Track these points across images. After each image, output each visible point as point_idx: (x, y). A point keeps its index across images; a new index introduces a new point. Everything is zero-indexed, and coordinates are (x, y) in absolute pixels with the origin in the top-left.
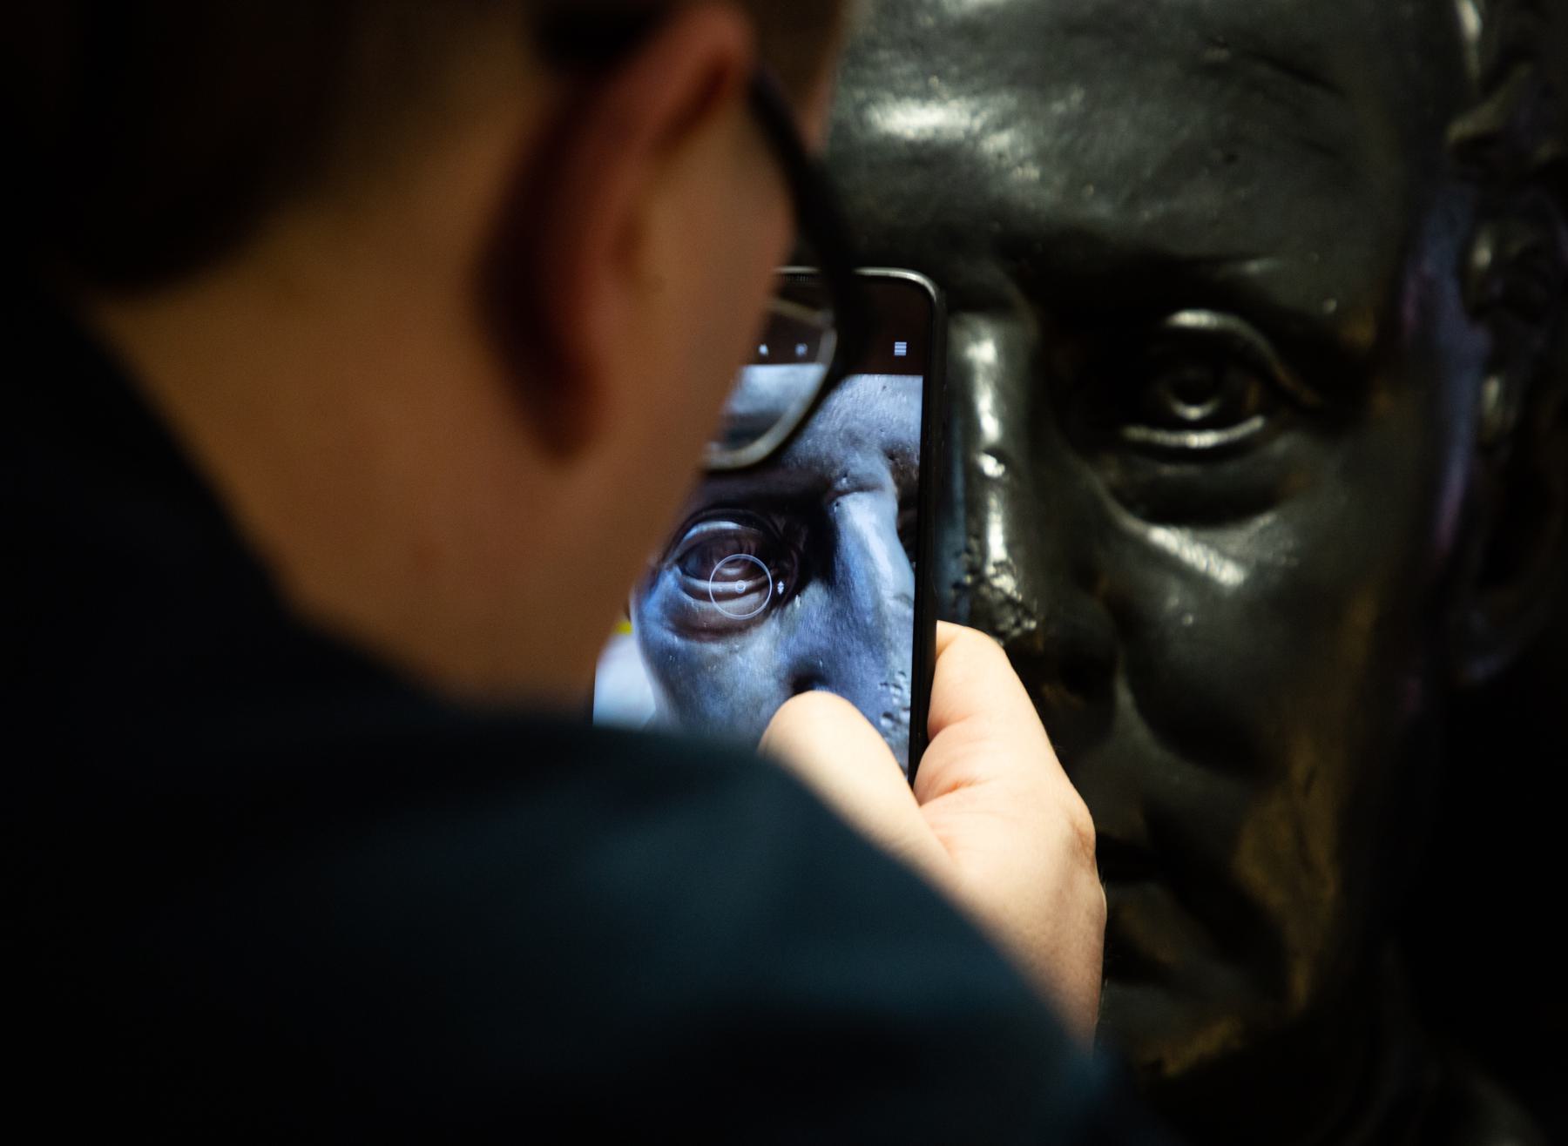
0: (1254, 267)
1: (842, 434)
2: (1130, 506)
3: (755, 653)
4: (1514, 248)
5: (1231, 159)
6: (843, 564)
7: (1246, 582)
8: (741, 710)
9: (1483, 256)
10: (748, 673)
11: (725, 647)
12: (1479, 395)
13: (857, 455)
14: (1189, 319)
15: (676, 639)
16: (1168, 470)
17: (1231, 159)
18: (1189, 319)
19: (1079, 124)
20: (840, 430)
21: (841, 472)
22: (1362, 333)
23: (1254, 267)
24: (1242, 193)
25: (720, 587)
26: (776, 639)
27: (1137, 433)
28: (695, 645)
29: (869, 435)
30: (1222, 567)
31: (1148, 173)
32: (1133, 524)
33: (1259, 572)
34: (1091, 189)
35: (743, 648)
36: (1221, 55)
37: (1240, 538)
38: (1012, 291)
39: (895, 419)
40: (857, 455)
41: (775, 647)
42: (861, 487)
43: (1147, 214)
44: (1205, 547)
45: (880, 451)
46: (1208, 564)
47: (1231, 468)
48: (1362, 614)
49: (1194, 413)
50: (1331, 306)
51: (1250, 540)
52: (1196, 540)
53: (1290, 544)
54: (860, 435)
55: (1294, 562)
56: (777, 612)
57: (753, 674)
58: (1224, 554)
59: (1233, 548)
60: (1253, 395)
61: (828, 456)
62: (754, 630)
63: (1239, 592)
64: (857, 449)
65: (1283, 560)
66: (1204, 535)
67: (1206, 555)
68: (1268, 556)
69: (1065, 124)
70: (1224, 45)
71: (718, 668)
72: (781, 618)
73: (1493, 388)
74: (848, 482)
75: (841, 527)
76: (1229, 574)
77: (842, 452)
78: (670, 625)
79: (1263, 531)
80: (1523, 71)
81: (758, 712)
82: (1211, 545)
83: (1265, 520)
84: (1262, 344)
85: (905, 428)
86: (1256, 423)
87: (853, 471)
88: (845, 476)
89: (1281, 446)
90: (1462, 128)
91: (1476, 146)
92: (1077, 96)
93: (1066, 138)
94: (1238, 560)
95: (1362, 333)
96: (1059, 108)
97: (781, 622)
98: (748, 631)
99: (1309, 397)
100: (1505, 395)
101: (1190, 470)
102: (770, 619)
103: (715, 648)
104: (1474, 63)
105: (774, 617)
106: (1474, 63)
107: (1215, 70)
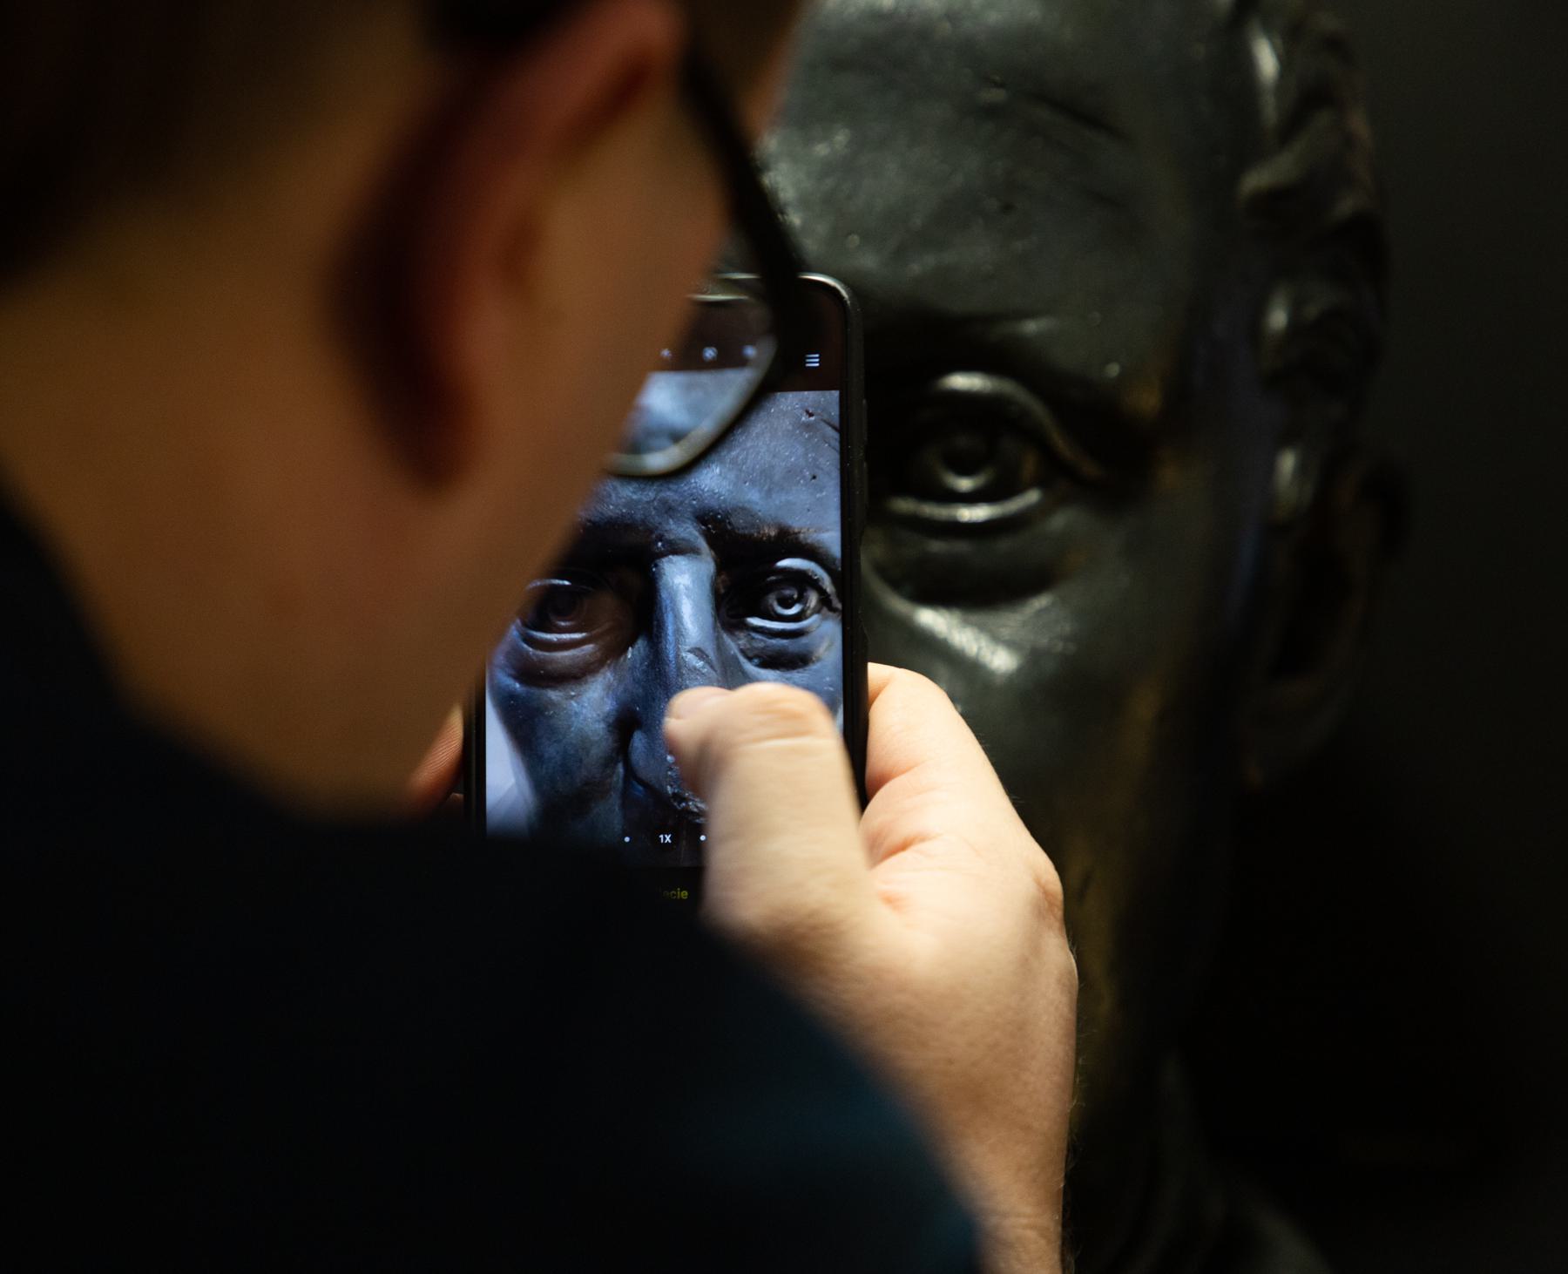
0: (1031, 327)
1: (656, 503)
2: (896, 585)
3: (589, 699)
4: (1312, 311)
5: (1007, 208)
6: (658, 621)
7: (1020, 670)
8: (572, 752)
9: (1278, 318)
10: (581, 718)
11: (561, 694)
12: (1270, 468)
13: (671, 521)
14: (961, 381)
15: (518, 685)
16: (937, 546)
17: (1007, 208)
18: (961, 381)
19: (845, 167)
20: (655, 499)
21: (657, 537)
22: (1147, 400)
23: (1031, 327)
24: (1019, 245)
25: (553, 637)
26: (609, 687)
27: (904, 505)
28: (535, 691)
29: (682, 502)
30: (993, 653)
31: (917, 221)
32: (898, 604)
33: (1033, 658)
34: (855, 239)
35: (578, 695)
36: (996, 95)
37: (1014, 620)
38: (702, 544)
39: (706, 489)
40: (671, 521)
41: (608, 694)
42: (677, 549)
43: (919, 266)
44: (976, 631)
45: (692, 518)
46: (980, 649)
47: (1004, 545)
48: (1144, 706)
49: (965, 484)
50: (1114, 370)
51: (1024, 624)
52: (966, 623)
53: (1067, 628)
54: (673, 504)
55: (1072, 648)
56: (611, 662)
57: (585, 720)
58: (996, 639)
59: (1005, 632)
60: (1030, 465)
61: (643, 522)
62: (590, 679)
63: (1011, 679)
64: (671, 516)
65: (1060, 646)
66: (975, 618)
67: (977, 640)
68: (1044, 641)
69: (828, 169)
70: (1001, 85)
71: (555, 712)
72: (615, 668)
73: (1287, 463)
74: (663, 545)
75: (661, 583)
76: (1001, 661)
77: (657, 519)
78: (513, 672)
79: (1040, 612)
80: (1323, 119)
81: (588, 755)
82: (982, 628)
83: (1041, 602)
84: (1038, 409)
85: (716, 496)
86: (1032, 497)
87: (667, 536)
88: (661, 541)
89: (1059, 521)
90: (1257, 179)
91: (1272, 200)
92: (841, 138)
93: (829, 183)
94: (1011, 645)
95: (1147, 400)
96: (821, 150)
97: (615, 671)
98: (584, 679)
99: (1090, 469)
100: (1302, 469)
101: (961, 547)
102: (606, 668)
103: (554, 695)
104: (1270, 110)
105: (609, 666)
106: (1270, 110)
107: (990, 112)
